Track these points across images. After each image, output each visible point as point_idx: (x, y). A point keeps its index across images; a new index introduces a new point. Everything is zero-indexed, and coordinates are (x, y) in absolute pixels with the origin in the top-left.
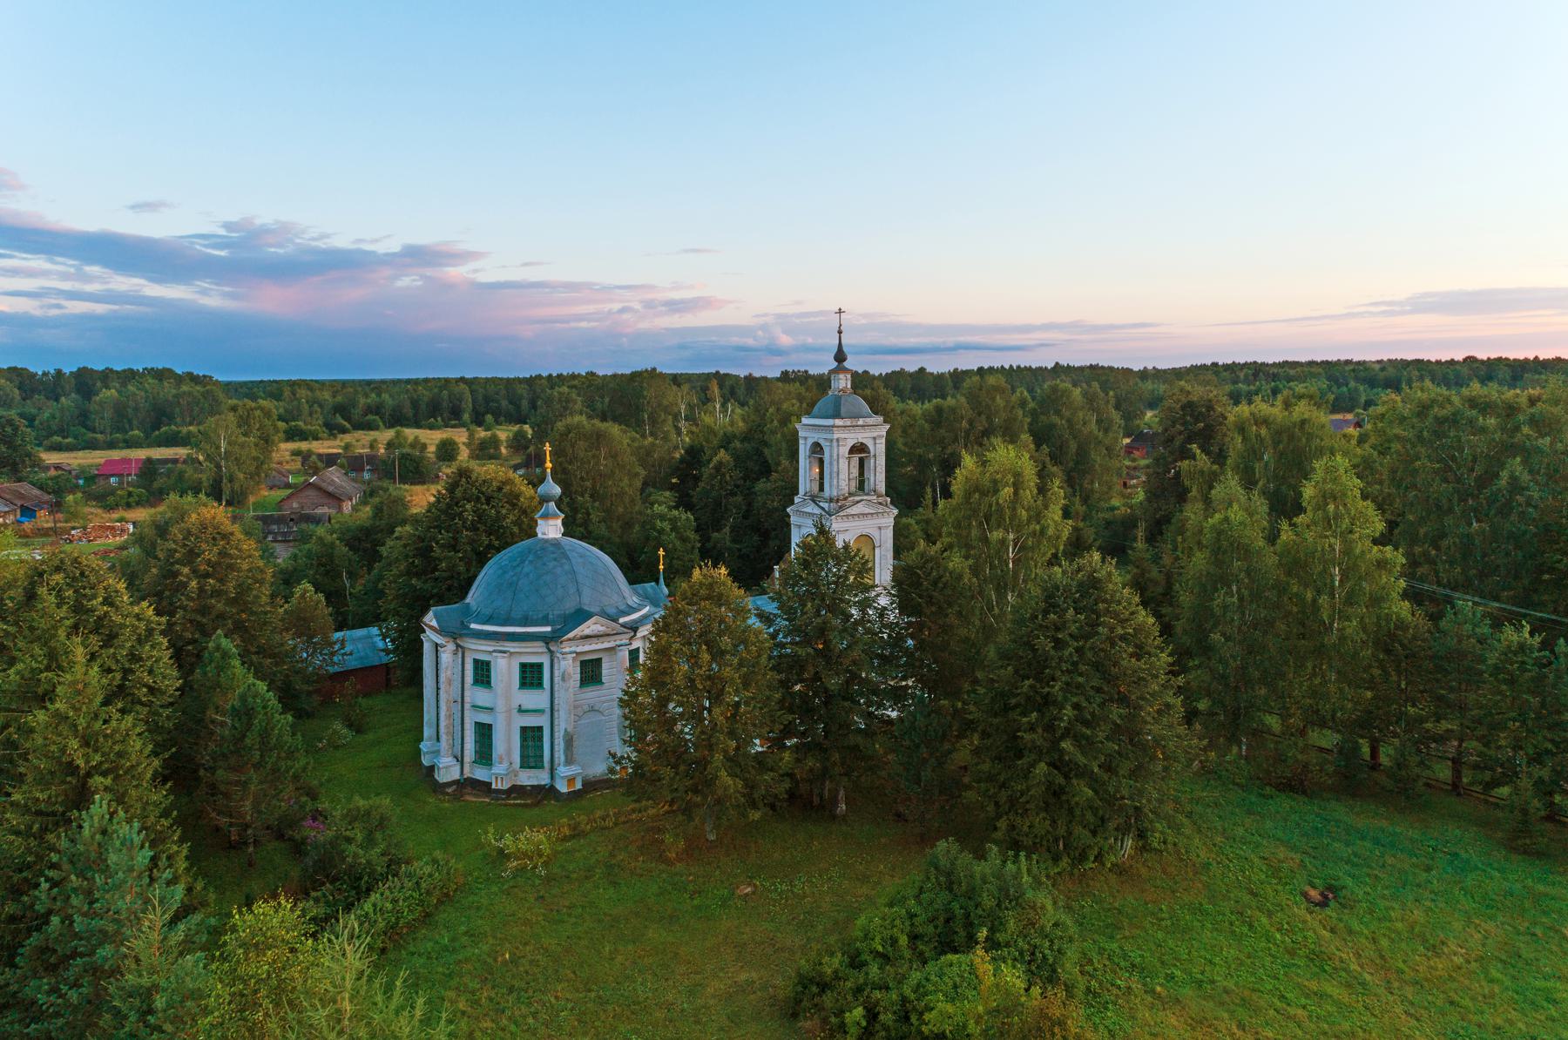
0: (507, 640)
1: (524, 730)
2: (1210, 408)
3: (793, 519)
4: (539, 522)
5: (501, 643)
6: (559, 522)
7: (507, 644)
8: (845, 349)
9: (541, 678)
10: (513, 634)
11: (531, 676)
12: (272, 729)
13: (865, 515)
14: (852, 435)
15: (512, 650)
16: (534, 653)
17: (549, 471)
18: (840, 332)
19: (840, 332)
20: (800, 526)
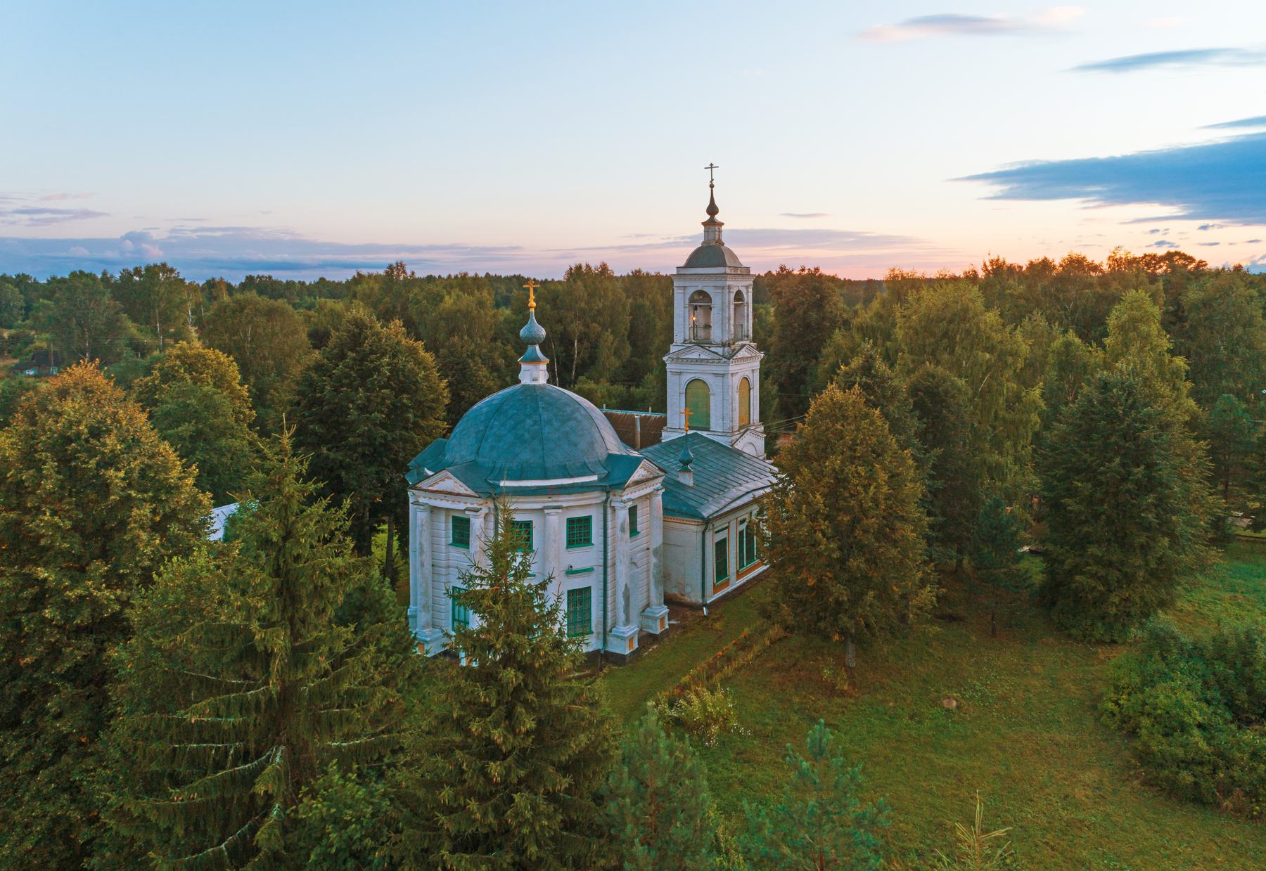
0: (560, 494)
1: (571, 593)
2: (408, 333)
3: (670, 367)
4: (524, 366)
5: (555, 498)
6: (543, 367)
7: (562, 498)
8: (717, 203)
9: (589, 534)
10: (573, 486)
11: (578, 532)
12: (884, 531)
13: (702, 360)
14: (694, 284)
15: (565, 505)
16: (586, 506)
17: (532, 310)
18: (712, 186)
19: (712, 186)
20: (680, 373)
